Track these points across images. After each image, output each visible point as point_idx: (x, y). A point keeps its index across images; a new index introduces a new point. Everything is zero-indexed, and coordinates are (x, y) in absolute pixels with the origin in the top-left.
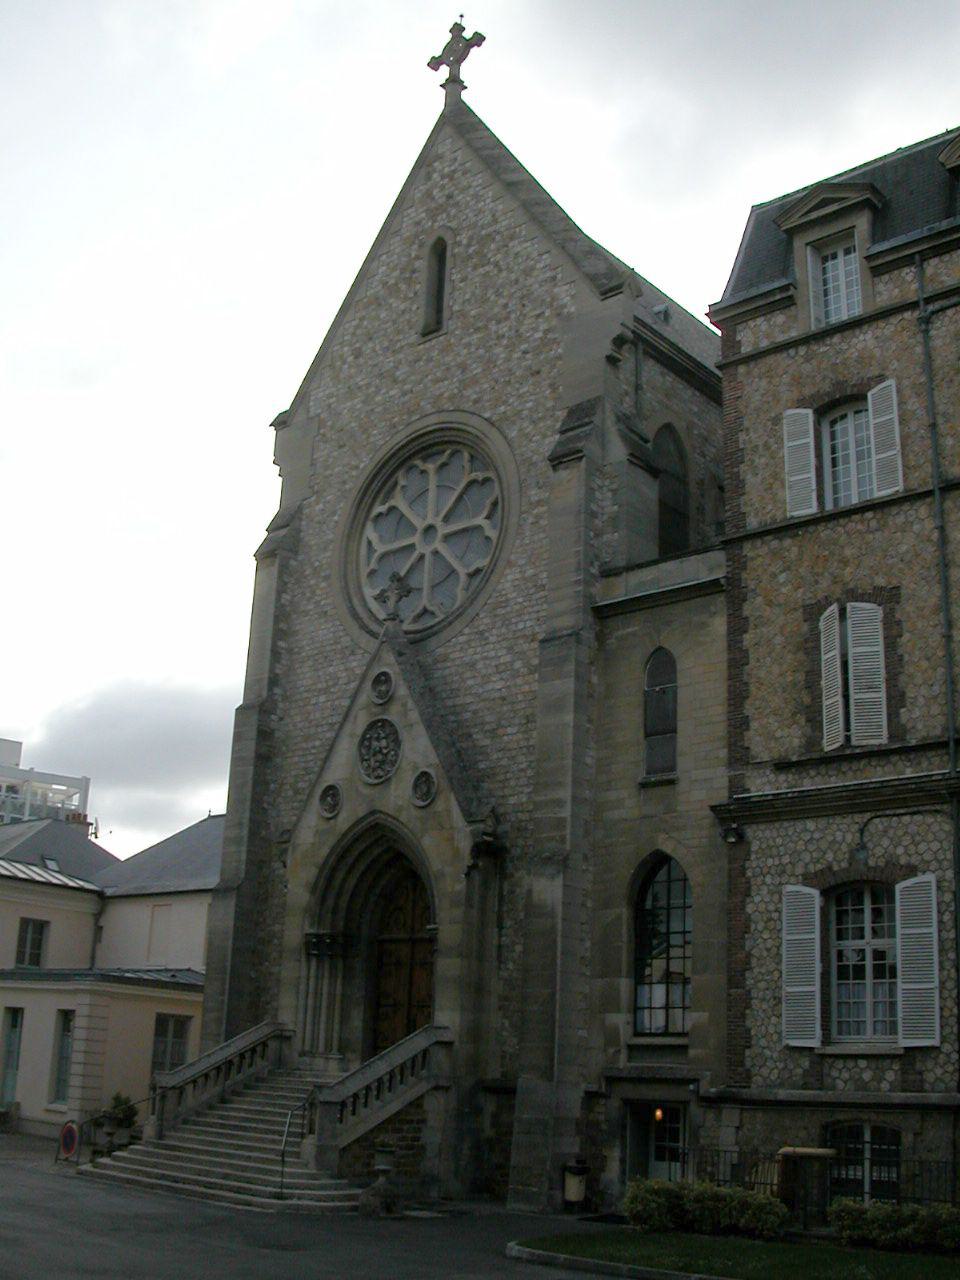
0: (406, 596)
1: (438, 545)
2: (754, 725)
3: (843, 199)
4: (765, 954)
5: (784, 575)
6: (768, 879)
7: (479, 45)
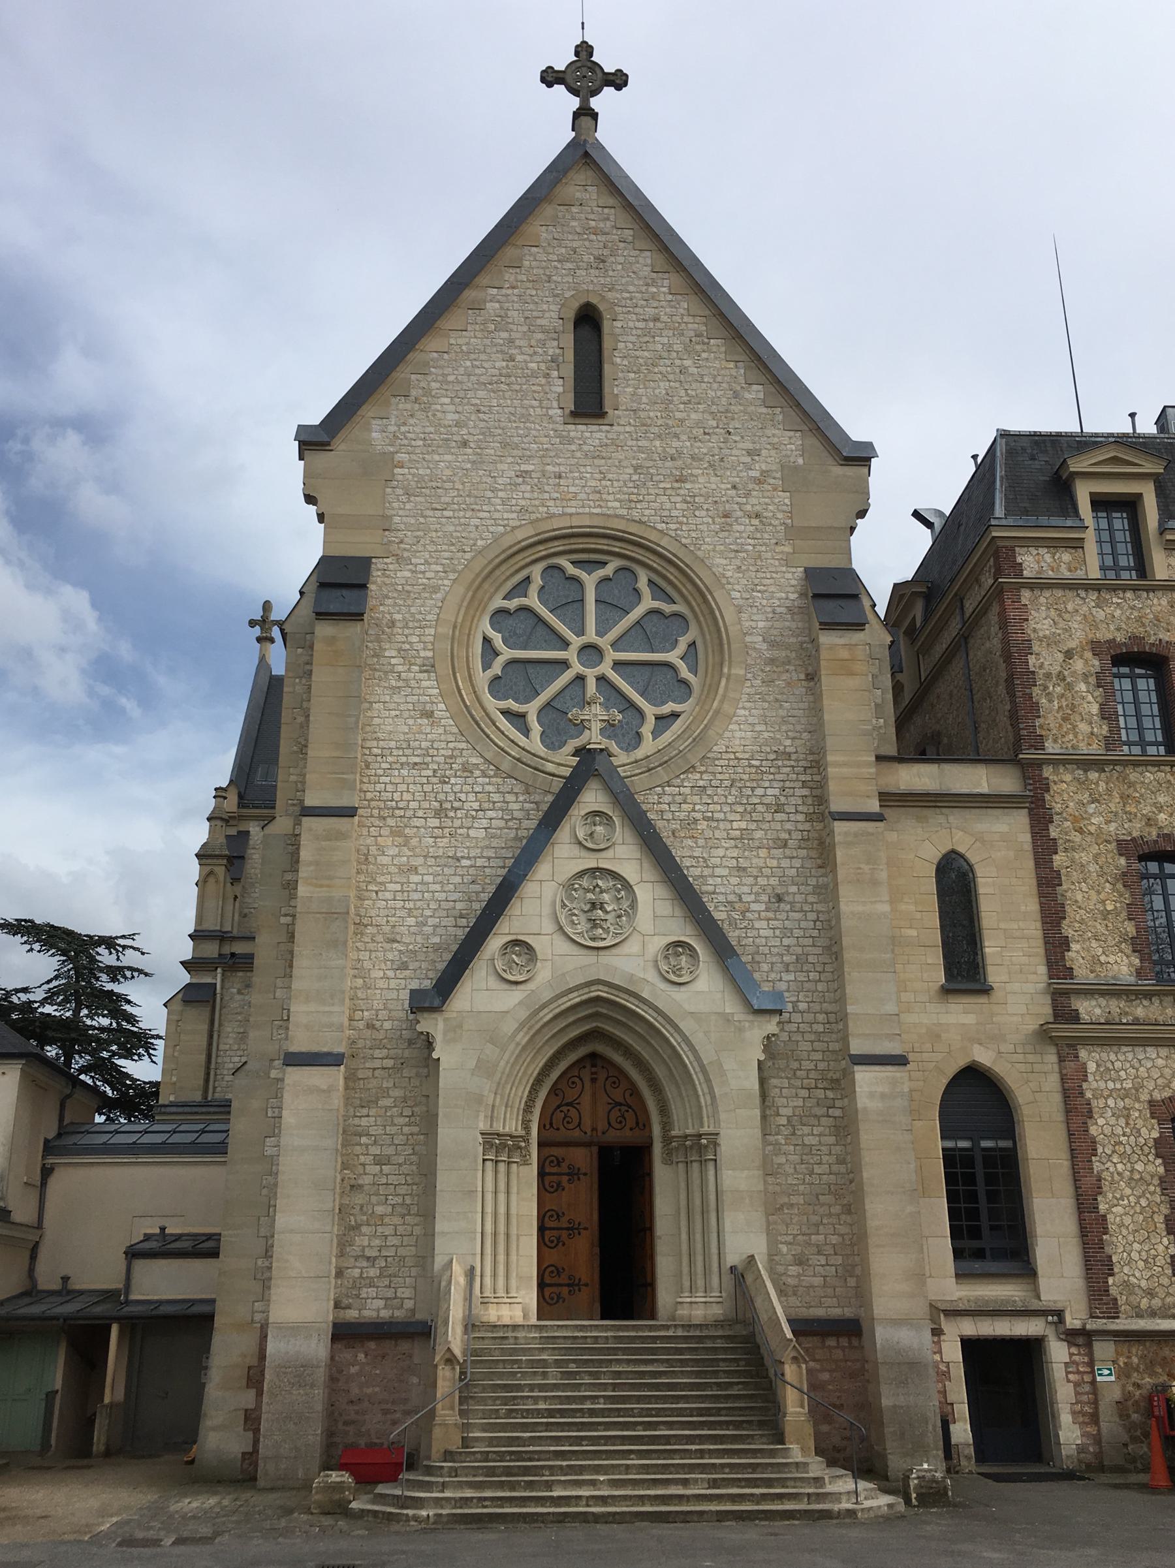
0: (591, 55)
1: (591, 674)
2: (1075, 947)
3: (1136, 465)
4: (1116, 1177)
5: (1093, 806)
6: (1111, 1102)
7: (619, 88)
